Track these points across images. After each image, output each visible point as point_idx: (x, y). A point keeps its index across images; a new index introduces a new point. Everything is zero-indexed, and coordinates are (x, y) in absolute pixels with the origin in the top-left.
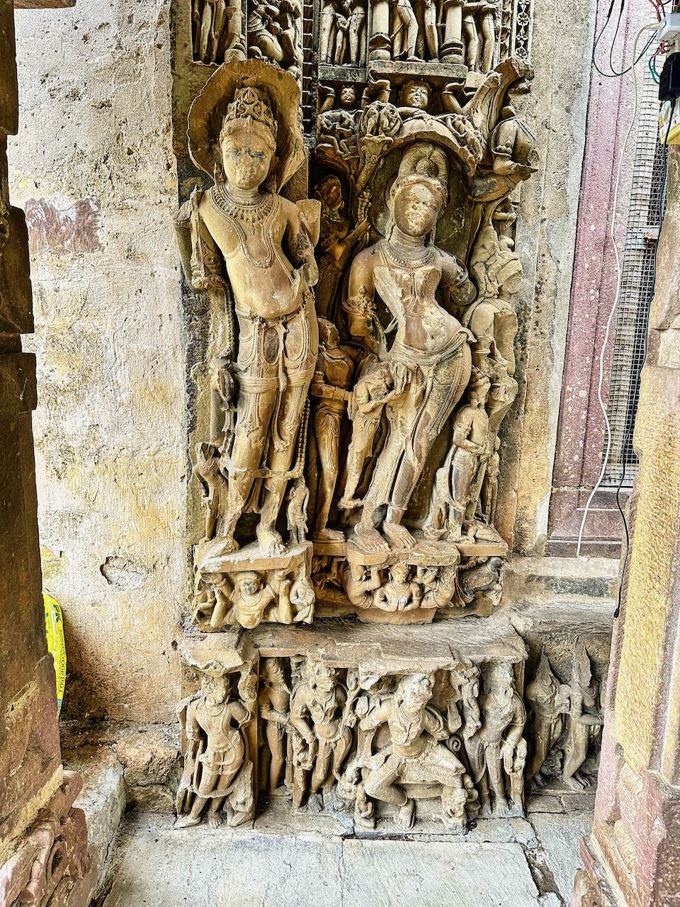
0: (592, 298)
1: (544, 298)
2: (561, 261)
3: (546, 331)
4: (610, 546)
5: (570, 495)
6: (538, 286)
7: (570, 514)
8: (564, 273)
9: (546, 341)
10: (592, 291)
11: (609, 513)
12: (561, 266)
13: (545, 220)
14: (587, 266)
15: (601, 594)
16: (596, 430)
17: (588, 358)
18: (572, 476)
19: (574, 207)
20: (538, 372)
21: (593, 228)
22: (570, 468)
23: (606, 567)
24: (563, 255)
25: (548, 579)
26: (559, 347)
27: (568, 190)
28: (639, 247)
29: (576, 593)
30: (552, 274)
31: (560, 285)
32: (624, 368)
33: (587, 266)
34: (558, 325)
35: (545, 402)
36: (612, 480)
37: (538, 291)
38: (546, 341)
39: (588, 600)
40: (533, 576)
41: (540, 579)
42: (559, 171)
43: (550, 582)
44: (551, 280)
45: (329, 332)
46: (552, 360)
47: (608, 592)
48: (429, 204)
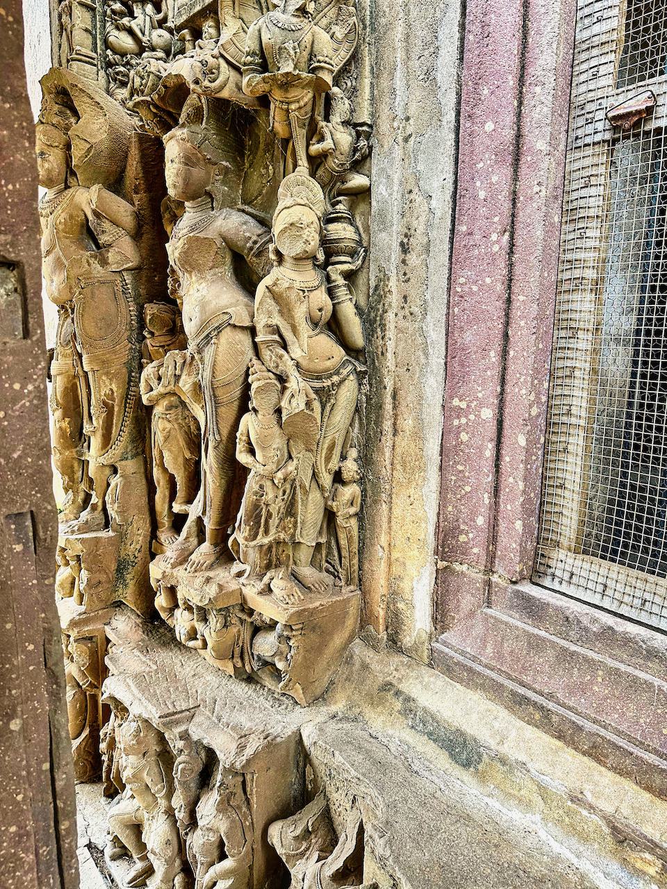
0: (496, 248)
1: (413, 259)
2: (434, 196)
3: (417, 309)
4: (514, 694)
5: (472, 581)
6: (405, 240)
7: (472, 614)
8: (438, 214)
9: (416, 325)
10: (494, 237)
11: (530, 635)
12: (434, 203)
13: (410, 136)
14: (482, 194)
15: (466, 765)
16: (511, 480)
17: (492, 354)
18: (475, 550)
19: (450, 100)
20: (408, 374)
21: (489, 126)
22: (471, 535)
23: (496, 725)
24: (435, 185)
25: (408, 699)
26: (436, 335)
27: (439, 79)
28: (598, 137)
29: (435, 741)
30: (423, 219)
31: (434, 234)
32: (577, 373)
33: (482, 194)
34: (432, 298)
35: (419, 420)
36: (557, 580)
37: (405, 248)
38: (416, 325)
39: (442, 760)
40: (391, 684)
41: (398, 693)
42: (426, 53)
43: (409, 708)
44: (421, 229)
45: (149, 317)
46: (426, 355)
47: (480, 767)
48: (177, 160)
